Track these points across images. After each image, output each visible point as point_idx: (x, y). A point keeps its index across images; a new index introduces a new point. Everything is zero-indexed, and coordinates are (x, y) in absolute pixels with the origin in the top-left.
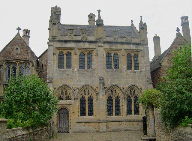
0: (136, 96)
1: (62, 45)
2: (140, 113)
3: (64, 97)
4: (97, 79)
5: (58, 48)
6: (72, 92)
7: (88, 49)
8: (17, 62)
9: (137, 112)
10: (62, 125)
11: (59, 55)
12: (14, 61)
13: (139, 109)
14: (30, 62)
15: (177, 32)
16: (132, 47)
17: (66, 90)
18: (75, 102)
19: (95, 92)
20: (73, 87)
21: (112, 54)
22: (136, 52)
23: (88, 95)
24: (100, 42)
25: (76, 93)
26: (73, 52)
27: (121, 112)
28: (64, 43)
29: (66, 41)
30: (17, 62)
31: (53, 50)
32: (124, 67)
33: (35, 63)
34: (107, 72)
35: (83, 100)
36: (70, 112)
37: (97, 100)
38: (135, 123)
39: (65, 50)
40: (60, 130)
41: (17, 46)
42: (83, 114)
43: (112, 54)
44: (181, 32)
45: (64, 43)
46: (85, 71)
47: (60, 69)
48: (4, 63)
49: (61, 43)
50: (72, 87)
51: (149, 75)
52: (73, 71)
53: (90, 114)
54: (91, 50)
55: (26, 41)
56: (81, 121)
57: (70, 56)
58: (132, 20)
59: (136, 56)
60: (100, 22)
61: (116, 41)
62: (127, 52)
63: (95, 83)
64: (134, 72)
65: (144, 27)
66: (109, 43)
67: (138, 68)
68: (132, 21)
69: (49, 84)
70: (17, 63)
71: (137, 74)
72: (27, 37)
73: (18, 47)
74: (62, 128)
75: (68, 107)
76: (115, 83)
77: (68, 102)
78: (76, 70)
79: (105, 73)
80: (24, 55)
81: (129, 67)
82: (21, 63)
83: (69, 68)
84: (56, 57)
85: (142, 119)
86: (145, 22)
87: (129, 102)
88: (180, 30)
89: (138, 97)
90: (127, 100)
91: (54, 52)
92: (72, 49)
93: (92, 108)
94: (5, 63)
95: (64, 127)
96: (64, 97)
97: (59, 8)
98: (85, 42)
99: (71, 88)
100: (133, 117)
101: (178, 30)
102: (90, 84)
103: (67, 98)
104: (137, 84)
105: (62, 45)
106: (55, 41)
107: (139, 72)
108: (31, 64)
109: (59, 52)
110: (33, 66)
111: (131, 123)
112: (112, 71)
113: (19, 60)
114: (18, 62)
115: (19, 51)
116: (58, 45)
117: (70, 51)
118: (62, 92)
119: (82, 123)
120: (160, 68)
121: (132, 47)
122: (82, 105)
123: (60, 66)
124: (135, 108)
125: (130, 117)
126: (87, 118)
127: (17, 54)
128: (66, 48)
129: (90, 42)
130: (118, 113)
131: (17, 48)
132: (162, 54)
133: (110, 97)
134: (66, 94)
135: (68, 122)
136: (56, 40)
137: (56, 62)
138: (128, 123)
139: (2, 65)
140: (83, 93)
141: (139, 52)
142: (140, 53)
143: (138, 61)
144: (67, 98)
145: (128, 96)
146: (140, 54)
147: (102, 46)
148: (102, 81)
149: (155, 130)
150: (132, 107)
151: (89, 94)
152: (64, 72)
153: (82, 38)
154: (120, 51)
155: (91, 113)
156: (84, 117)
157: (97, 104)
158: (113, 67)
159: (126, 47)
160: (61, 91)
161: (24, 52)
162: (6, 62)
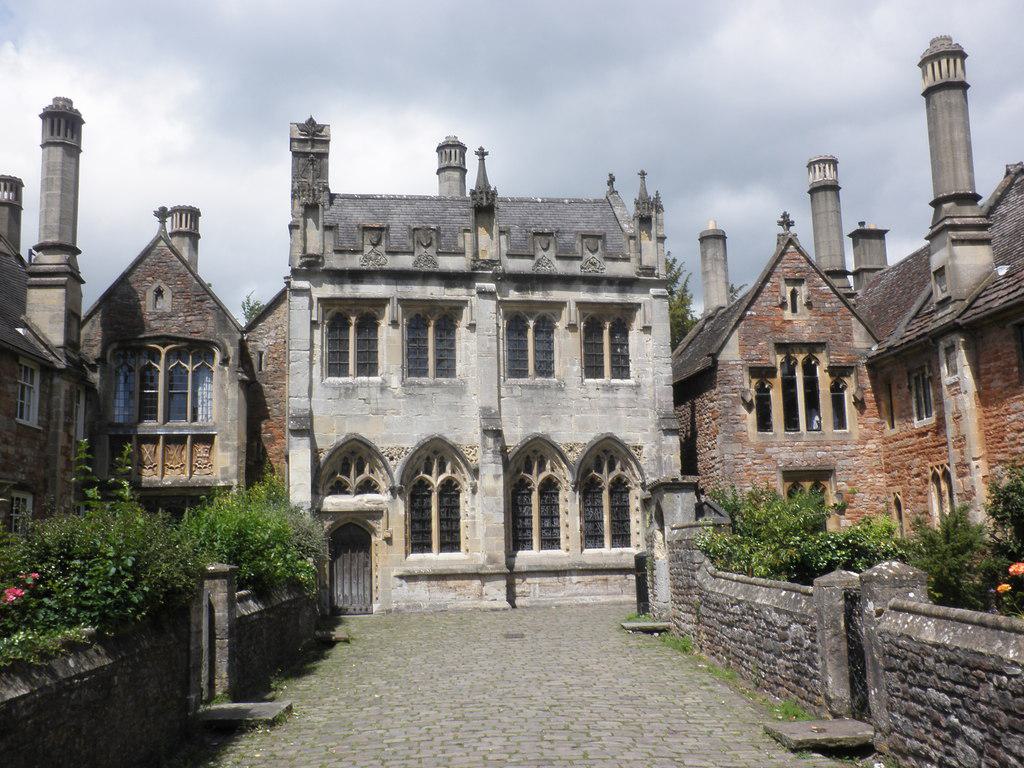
20: (386, 445)
29: (357, 276)
33: (232, 351)
42: (419, 541)
52: (383, 388)
61: (545, 270)
64: (609, 388)
71: (621, 394)
73: (163, 286)
78: (395, 382)
80: (189, 319)
92: (381, 303)
110: (225, 362)
127: (161, 317)
129: (450, 279)
156: (427, 555)
157: (473, 509)
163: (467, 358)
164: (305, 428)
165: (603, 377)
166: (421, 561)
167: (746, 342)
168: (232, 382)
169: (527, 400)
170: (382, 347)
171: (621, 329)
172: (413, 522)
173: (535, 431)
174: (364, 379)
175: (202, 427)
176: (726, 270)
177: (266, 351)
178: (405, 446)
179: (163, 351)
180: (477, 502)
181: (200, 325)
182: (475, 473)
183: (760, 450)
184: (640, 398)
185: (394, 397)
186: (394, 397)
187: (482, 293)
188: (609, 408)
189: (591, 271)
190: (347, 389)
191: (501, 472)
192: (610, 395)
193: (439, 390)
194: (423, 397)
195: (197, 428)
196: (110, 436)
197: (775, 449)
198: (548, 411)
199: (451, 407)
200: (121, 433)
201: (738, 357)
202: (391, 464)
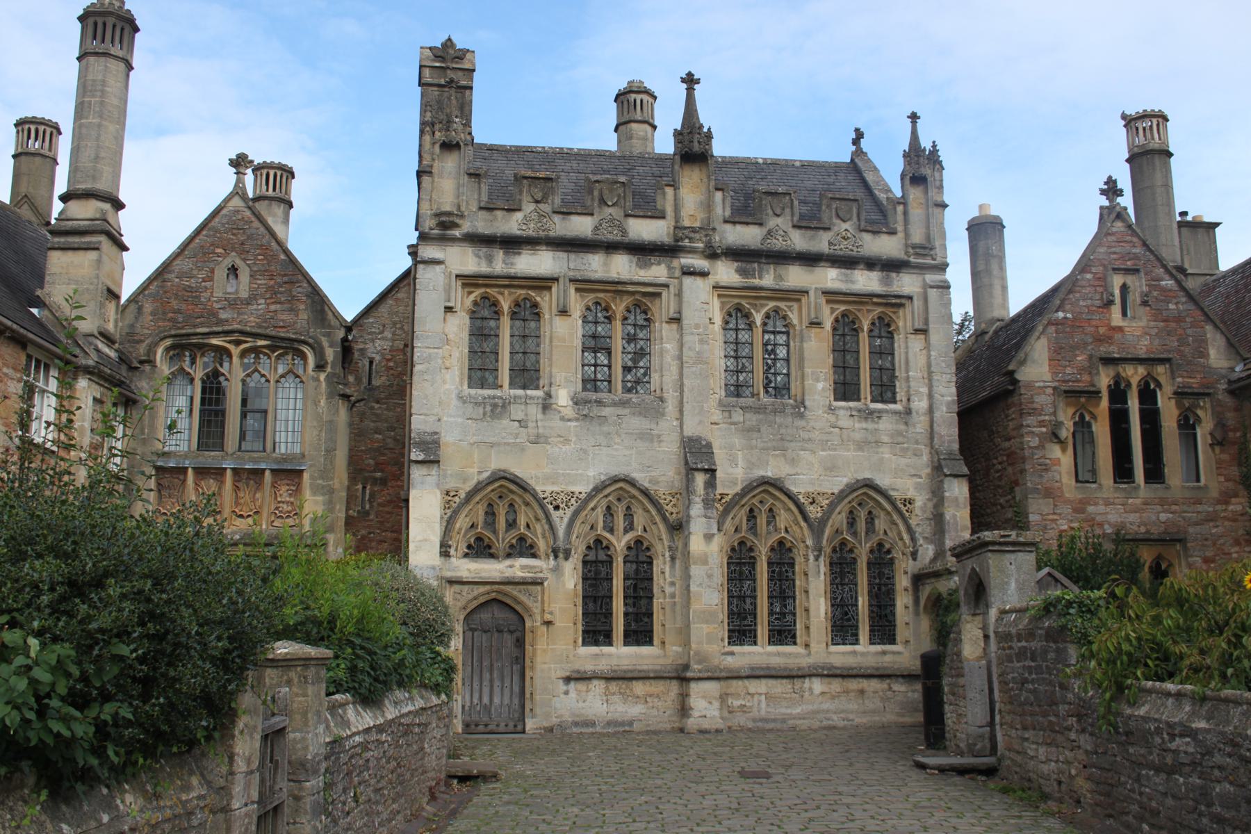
0: (880, 545)
1: (490, 259)
2: (901, 632)
3: (503, 539)
4: (670, 448)
5: (469, 281)
7: (630, 288)
8: (231, 347)
9: (884, 630)
10: (486, 690)
11: (473, 315)
13: (893, 614)
14: (306, 349)
15: (1107, 203)
16: (866, 281)
19: (664, 519)
20: (549, 488)
22: (879, 310)
23: (626, 531)
24: (692, 251)
26: (545, 302)
27: (799, 626)
28: (499, 255)
29: (512, 244)
30: (231, 347)
31: (448, 290)
32: (820, 386)
33: (330, 354)
34: (726, 414)
38: (874, 684)
39: (506, 292)
40: (475, 717)
41: (233, 258)
42: (597, 632)
44: (1126, 201)
45: (501, 252)
46: (615, 404)
47: (480, 391)
48: (160, 351)
49: (484, 250)
51: (949, 432)
53: (635, 632)
54: (645, 294)
55: (278, 229)
56: (589, 667)
57: (533, 324)
58: (857, 130)
59: (884, 328)
60: (696, 144)
61: (778, 244)
62: (835, 306)
64: (869, 415)
65: (926, 171)
66: (738, 254)
67: (894, 393)
68: (859, 135)
70: (235, 351)
72: (279, 210)
74: (487, 709)
75: (524, 598)
76: (770, 473)
77: (523, 567)
78: (563, 398)
80: (273, 307)
81: (845, 389)
82: (256, 350)
83: (524, 387)
84: (458, 327)
85: (916, 665)
86: (934, 146)
87: (842, 574)
88: (1119, 193)
89: (887, 546)
90: (831, 564)
92: (543, 283)
94: (168, 349)
95: (497, 700)
96: (503, 539)
97: (462, 54)
98: (611, 247)
100: (864, 651)
101: (1111, 189)
102: (638, 476)
103: (512, 546)
104: (883, 481)
105: (490, 259)
106: (454, 240)
107: (896, 413)
109: (472, 297)
110: (320, 367)
111: (854, 684)
113: (242, 333)
114: (238, 343)
115: (243, 286)
116: (465, 260)
118: (491, 513)
119: (595, 682)
120: (1008, 394)
121: (866, 281)
122: (591, 586)
124: (870, 605)
125: (841, 655)
127: (233, 303)
128: (513, 281)
129: (643, 251)
130: (783, 633)
131: (234, 270)
132: (1018, 316)
133: (742, 543)
135: (516, 678)
136: (457, 233)
138: (836, 685)
139: (151, 362)
140: (601, 524)
141: (901, 305)
142: (901, 312)
143: (893, 354)
144: (512, 546)
145: (836, 542)
146: (905, 320)
147: (703, 274)
149: (992, 724)
150: (860, 603)
151: (630, 527)
152: (498, 409)
153: (596, 228)
154: (799, 300)
155: (640, 633)
156: (606, 649)
158: (505, 376)
159: (831, 277)
161: (269, 288)
162: (168, 342)
169: (750, 430)
173: (762, 473)
177: (377, 358)
181: (286, 317)
182: (678, 528)
184: (911, 429)
185: (562, 419)
186: (562, 419)
188: (867, 442)
190: (495, 406)
192: (870, 425)
193: (626, 411)
195: (277, 461)
198: (781, 446)
202: (555, 515)
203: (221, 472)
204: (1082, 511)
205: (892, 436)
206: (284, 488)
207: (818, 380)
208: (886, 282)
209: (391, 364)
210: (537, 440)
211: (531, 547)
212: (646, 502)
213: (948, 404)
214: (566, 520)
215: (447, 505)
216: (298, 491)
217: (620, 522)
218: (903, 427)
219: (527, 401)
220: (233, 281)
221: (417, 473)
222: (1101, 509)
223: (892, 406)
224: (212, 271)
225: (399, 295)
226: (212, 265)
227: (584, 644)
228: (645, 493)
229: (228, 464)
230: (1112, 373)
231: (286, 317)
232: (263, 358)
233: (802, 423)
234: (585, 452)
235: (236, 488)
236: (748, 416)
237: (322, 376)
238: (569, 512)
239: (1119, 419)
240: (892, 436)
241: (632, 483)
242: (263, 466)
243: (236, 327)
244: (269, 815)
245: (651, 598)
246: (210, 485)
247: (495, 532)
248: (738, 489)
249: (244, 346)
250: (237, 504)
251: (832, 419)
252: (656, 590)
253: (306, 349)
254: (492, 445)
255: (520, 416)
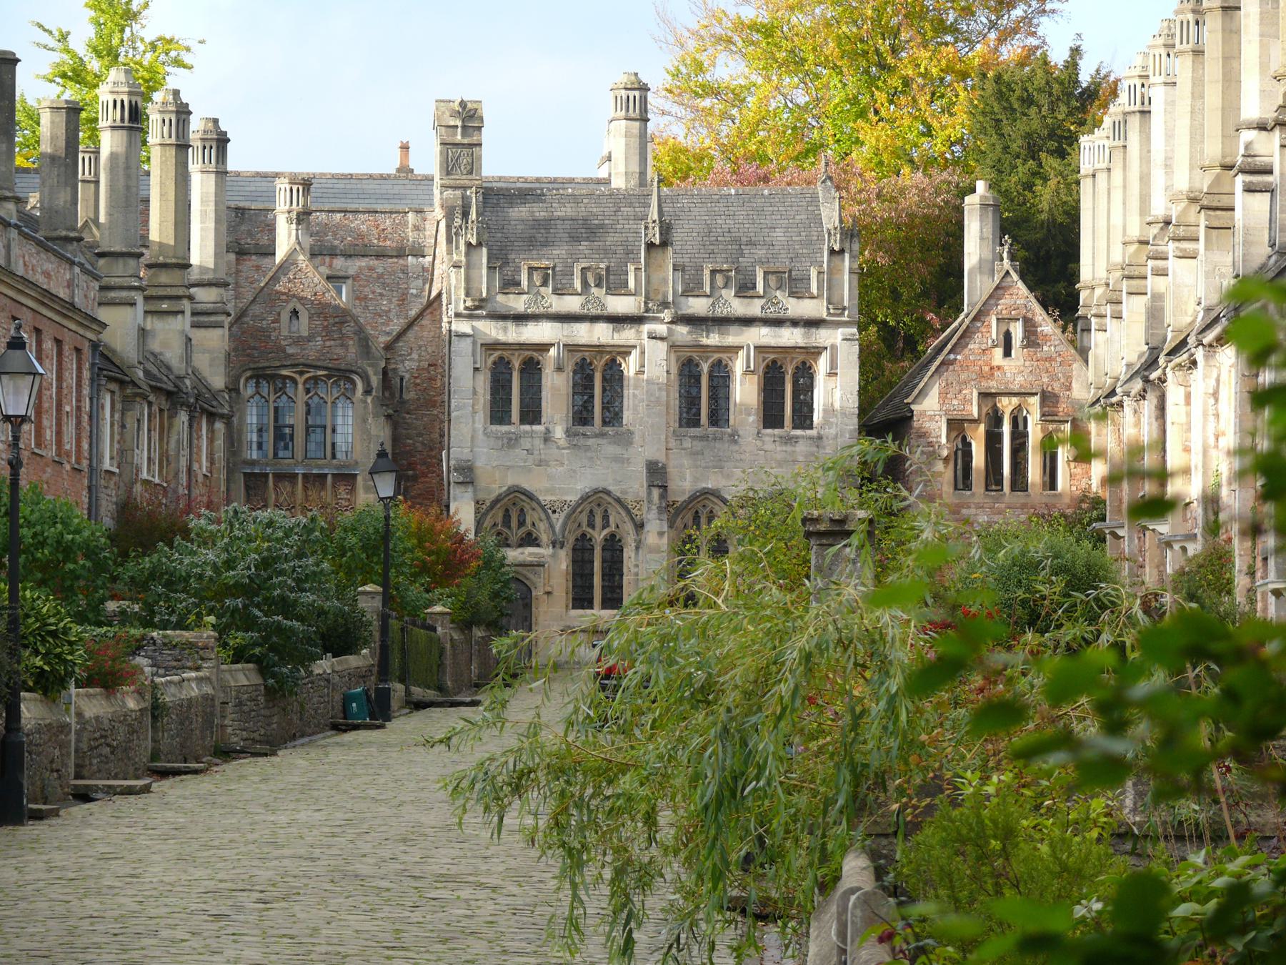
1: (505, 330)
3: (516, 534)
6: (543, 516)
12: (285, 372)
14: (355, 377)
17: (522, 510)
18: (553, 556)
19: (632, 519)
20: (549, 498)
21: (705, 368)
23: (604, 528)
24: (655, 319)
25: (558, 520)
28: (511, 326)
29: (521, 318)
33: (375, 380)
35: (583, 550)
36: (538, 593)
37: (637, 548)
42: (581, 599)
43: (705, 368)
46: (596, 436)
49: (501, 323)
50: (545, 498)
52: (547, 438)
61: (721, 311)
63: (633, 485)
69: (462, 488)
70: (300, 380)
71: (801, 448)
73: (299, 307)
75: (531, 576)
77: (530, 554)
78: (559, 433)
79: (672, 444)
80: (328, 343)
82: (316, 379)
84: (483, 384)
91: (475, 362)
92: (544, 347)
93: (617, 578)
98: (594, 319)
99: (539, 503)
102: (611, 488)
105: (505, 330)
107: (811, 438)
108: (360, 386)
109: (492, 359)
110: (368, 392)
112: (704, 438)
117: (535, 354)
121: (790, 337)
123: (499, 414)
126: (599, 615)
127: (298, 341)
128: (522, 346)
129: (618, 320)
134: (522, 523)
137: (484, 396)
148: (657, 474)
153: (583, 306)
155: (613, 599)
156: (589, 612)
157: (637, 566)
159: (763, 335)
160: (501, 515)
162: (249, 374)
163: (635, 407)
164: (468, 475)
165: (782, 427)
166: (584, 617)
167: (943, 396)
168: (376, 416)
169: (697, 453)
170: (546, 395)
171: (805, 376)
172: (574, 575)
173: (704, 485)
174: (527, 427)
175: (343, 467)
176: (1125, 159)
177: (407, 376)
178: (568, 498)
179: (300, 380)
180: (641, 558)
181: (340, 351)
182: (640, 526)
183: (955, 511)
184: (822, 451)
185: (558, 448)
186: (558, 448)
187: (653, 337)
188: (786, 461)
189: (772, 312)
190: (510, 439)
191: (666, 529)
192: (789, 448)
193: (605, 441)
194: (588, 448)
195: (338, 467)
196: (245, 474)
197: (973, 511)
198: (719, 465)
199: (618, 459)
200: (257, 471)
201: (937, 407)
202: (554, 517)
203: (293, 477)
204: (958, 513)
205: (806, 456)
206: (342, 488)
207: (749, 415)
208: (806, 336)
209: (418, 381)
210: (540, 463)
211: (536, 539)
212: (618, 507)
213: (851, 431)
214: (561, 521)
215: (477, 511)
216: (353, 490)
217: (598, 521)
218: (815, 449)
219: (531, 435)
220: (295, 322)
221: (455, 491)
222: (973, 511)
223: (809, 432)
224: (279, 314)
225: (423, 322)
226: (278, 309)
227: (573, 608)
228: (618, 501)
229: (300, 471)
230: (990, 405)
231: (340, 351)
232: (321, 384)
233: (735, 448)
234: (574, 471)
235: (305, 488)
236: (695, 443)
237: (369, 399)
238: (563, 515)
239: (993, 441)
240: (806, 456)
241: (608, 493)
242: (326, 471)
243: (302, 360)
244: (1230, 9)
245: (622, 575)
246: (286, 487)
247: (509, 527)
248: (686, 497)
249: (307, 375)
250: (307, 500)
251: (759, 443)
252: (625, 570)
253: (355, 377)
254: (509, 468)
255: (528, 446)
